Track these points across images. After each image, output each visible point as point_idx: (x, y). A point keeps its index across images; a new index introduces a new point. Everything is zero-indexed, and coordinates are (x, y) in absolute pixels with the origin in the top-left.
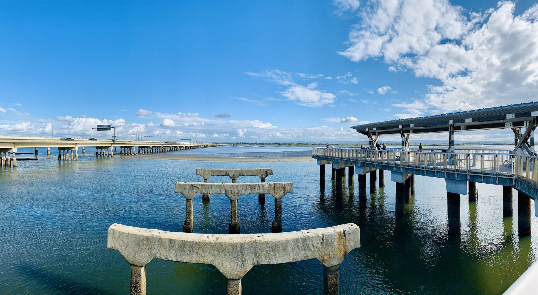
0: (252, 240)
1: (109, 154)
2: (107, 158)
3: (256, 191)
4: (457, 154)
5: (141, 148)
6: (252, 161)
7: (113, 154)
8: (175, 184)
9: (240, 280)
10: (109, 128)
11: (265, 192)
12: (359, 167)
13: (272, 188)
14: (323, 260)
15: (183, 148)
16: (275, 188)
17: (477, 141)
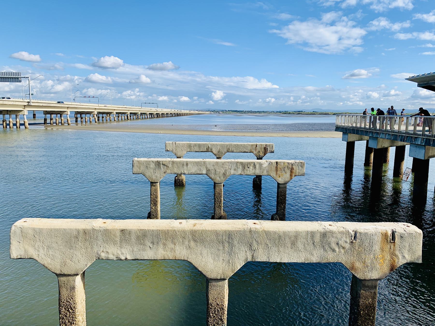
0: (245, 227)
1: (21, 124)
2: (17, 130)
3: (251, 171)
4: (408, 117)
5: (79, 115)
6: (244, 136)
7: (29, 124)
8: (133, 161)
9: (227, 281)
11: (263, 172)
12: (417, 146)
13: (274, 168)
14: (353, 268)
15: (146, 117)
16: (279, 169)
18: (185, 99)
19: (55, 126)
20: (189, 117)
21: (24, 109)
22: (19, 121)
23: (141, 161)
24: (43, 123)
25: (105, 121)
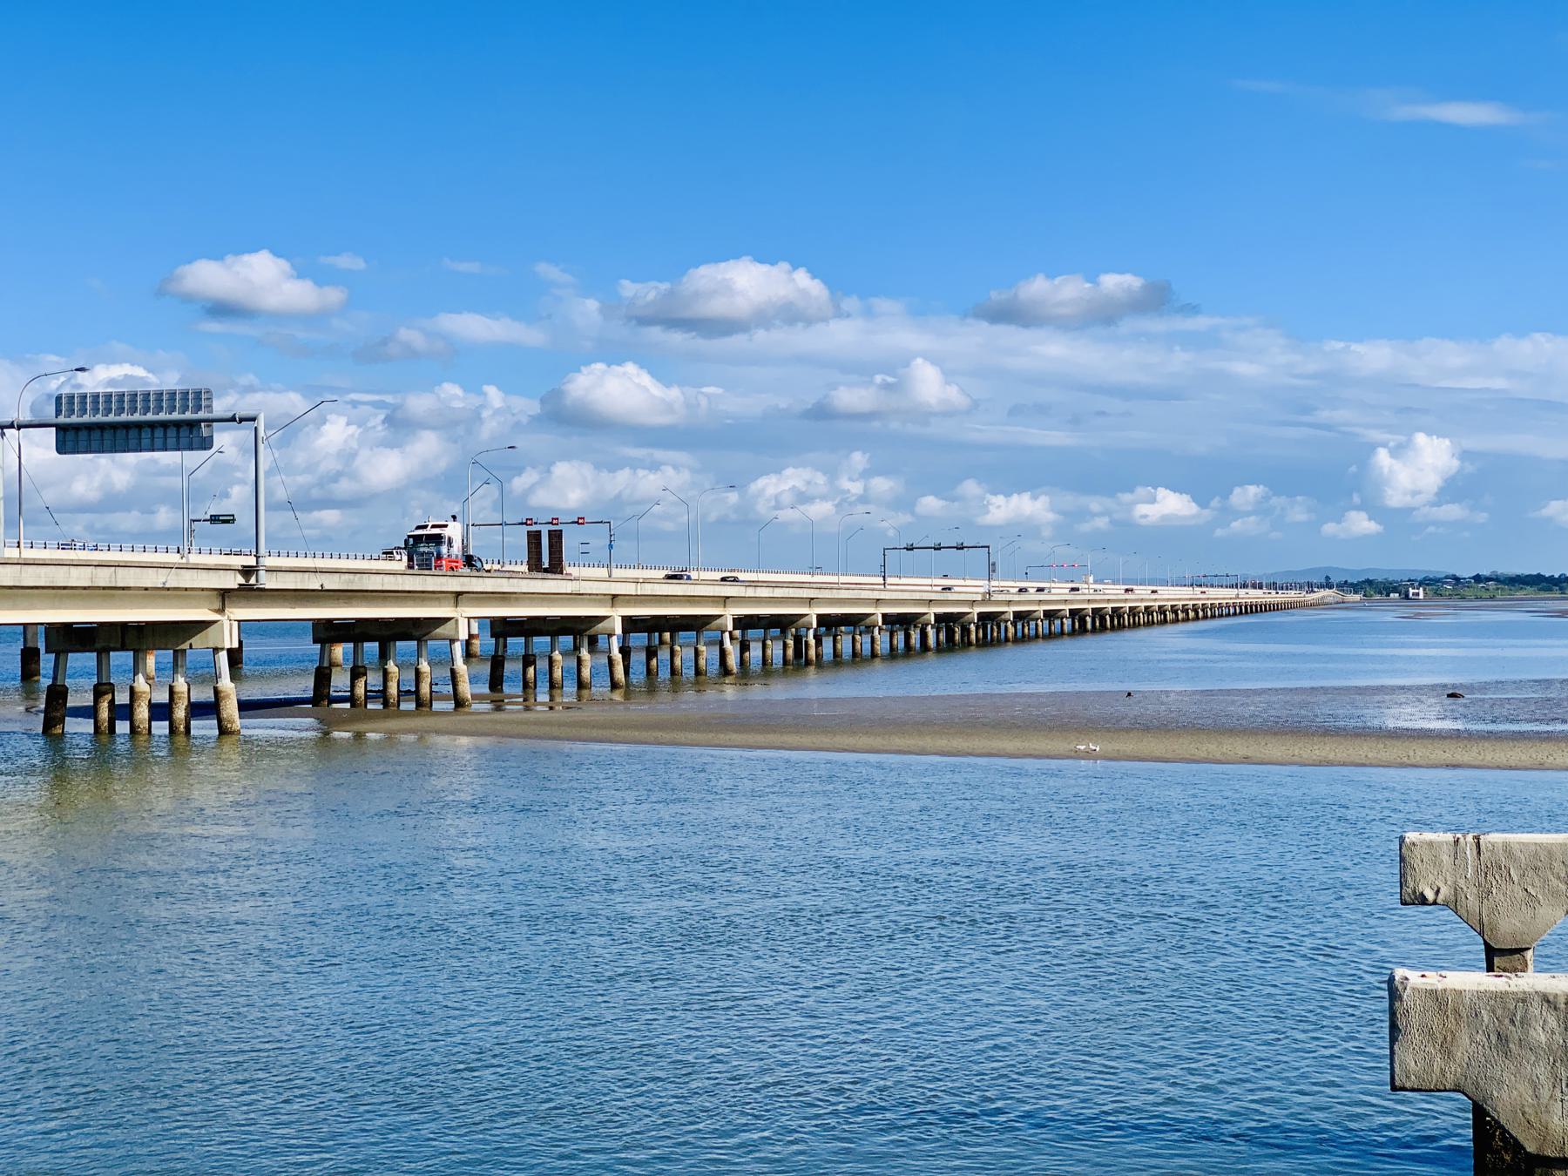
1: (199, 710)
2: (173, 751)
6: (1541, 767)
7: (245, 707)
10: (193, 425)
18: (1170, 505)
19: (374, 715)
20: (1202, 633)
21: (221, 611)
22: (185, 688)
23: (1459, 993)
24: (310, 694)
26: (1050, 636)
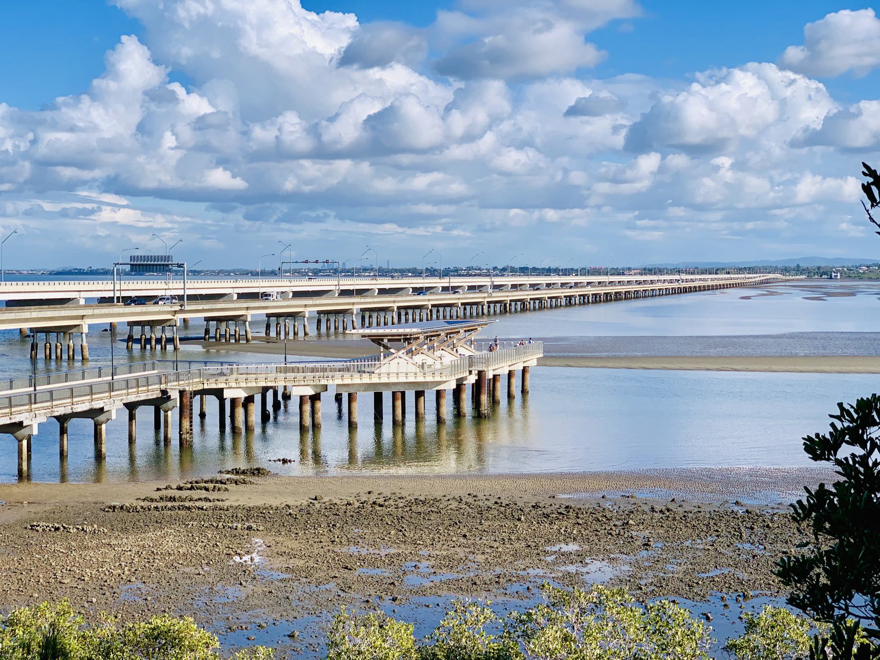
7: (181, 339)
17: (61, 268)
19: (223, 344)
25: (410, 320)
26: (652, 296)
